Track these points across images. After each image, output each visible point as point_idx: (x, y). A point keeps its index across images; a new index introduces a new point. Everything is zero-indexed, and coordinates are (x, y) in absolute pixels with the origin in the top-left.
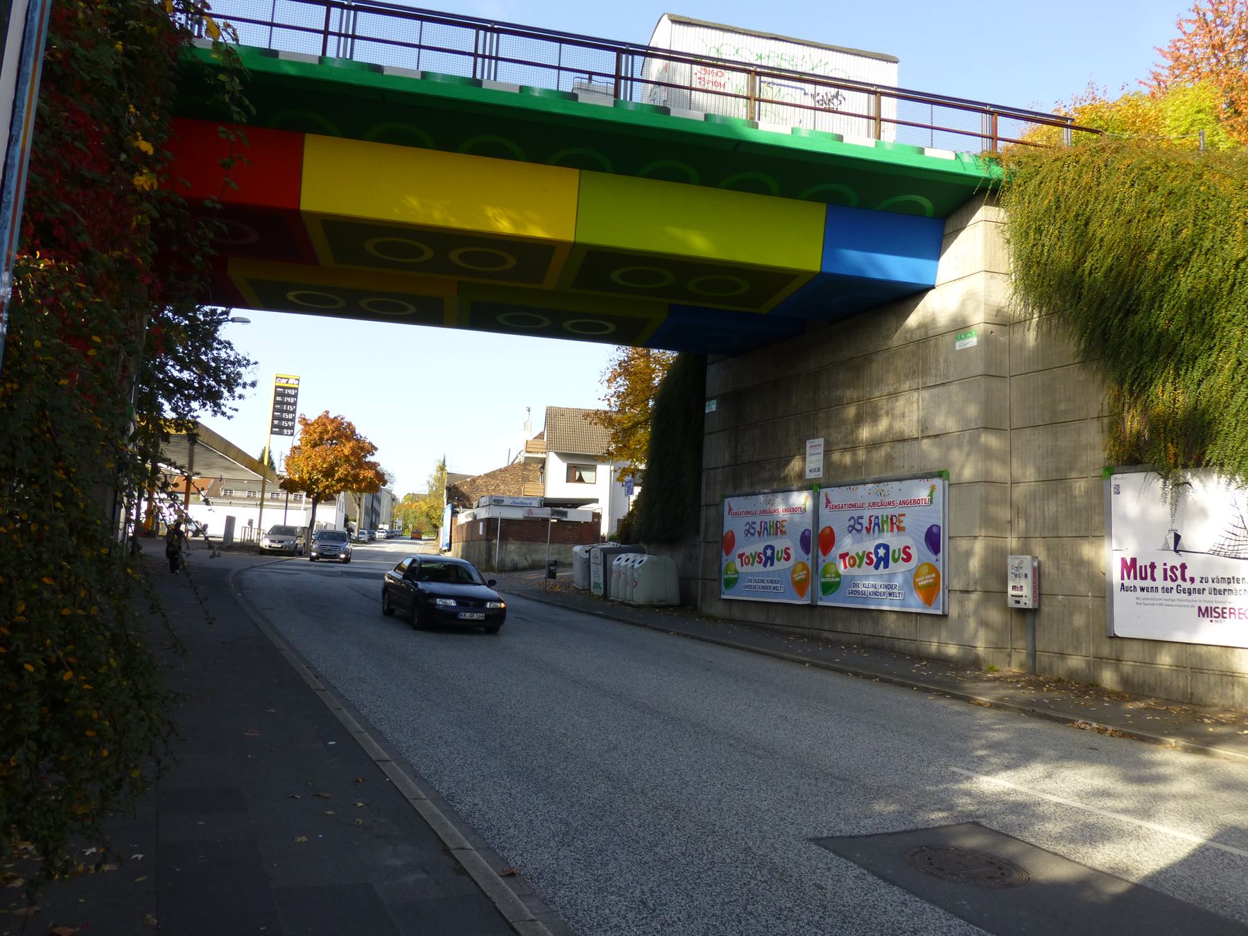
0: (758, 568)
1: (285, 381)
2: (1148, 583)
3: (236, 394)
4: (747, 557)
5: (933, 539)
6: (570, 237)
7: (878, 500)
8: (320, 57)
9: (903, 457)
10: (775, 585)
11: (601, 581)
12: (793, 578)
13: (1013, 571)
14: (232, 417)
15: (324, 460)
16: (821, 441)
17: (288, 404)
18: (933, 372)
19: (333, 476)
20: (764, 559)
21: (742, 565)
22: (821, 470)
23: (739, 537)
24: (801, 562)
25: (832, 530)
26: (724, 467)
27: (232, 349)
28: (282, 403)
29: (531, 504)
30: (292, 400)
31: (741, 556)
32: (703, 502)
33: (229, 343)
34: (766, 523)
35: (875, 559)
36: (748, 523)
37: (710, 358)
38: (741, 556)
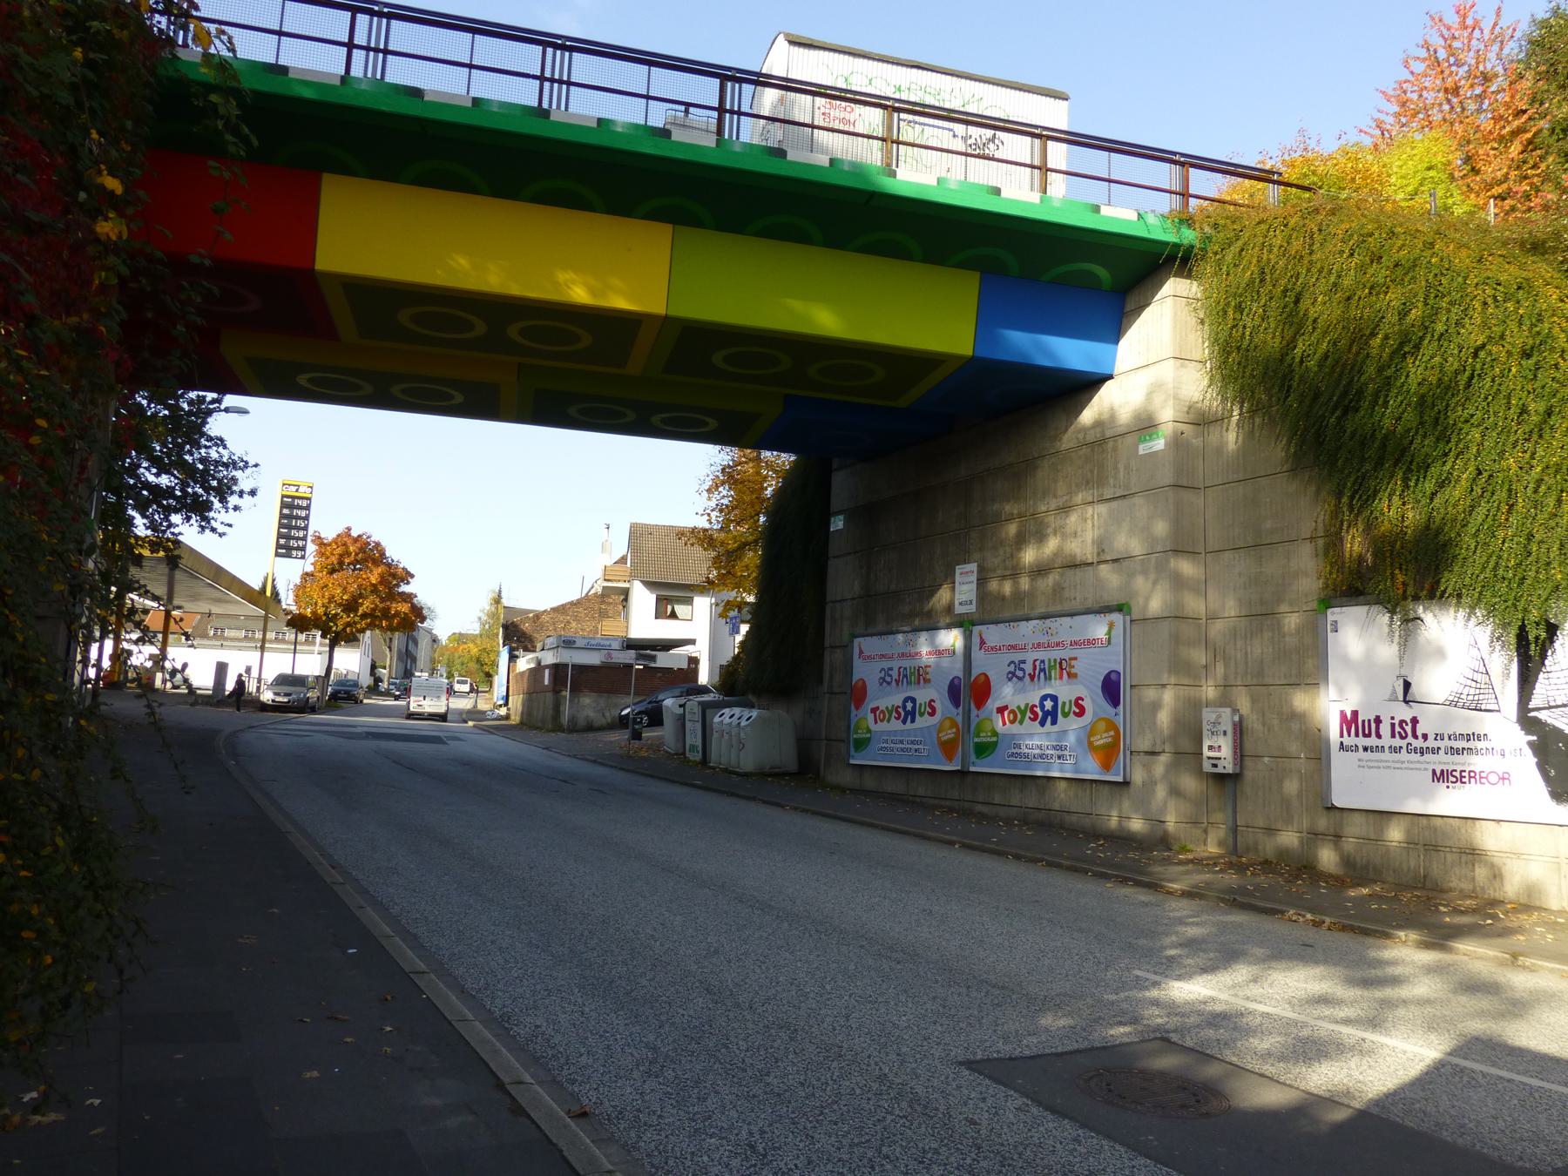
0: (896, 725)
1: (294, 488)
2: (1372, 741)
3: (230, 505)
4: (882, 712)
5: (1111, 689)
7: (1044, 640)
8: (342, 77)
9: (1075, 586)
10: (917, 747)
11: (699, 743)
12: (939, 738)
13: (1208, 727)
14: (224, 534)
15: (345, 590)
16: (973, 567)
17: (298, 518)
18: (1111, 481)
19: (356, 611)
20: (903, 714)
21: (876, 722)
22: (974, 602)
23: (873, 686)
24: (949, 718)
25: (864, 682)
26: (853, 599)
27: (225, 447)
28: (290, 517)
29: (610, 646)
30: (303, 513)
31: (874, 710)
32: (827, 644)
33: (221, 440)
34: (905, 669)
35: (1040, 714)
36: (883, 669)
37: (835, 463)
38: (874, 710)
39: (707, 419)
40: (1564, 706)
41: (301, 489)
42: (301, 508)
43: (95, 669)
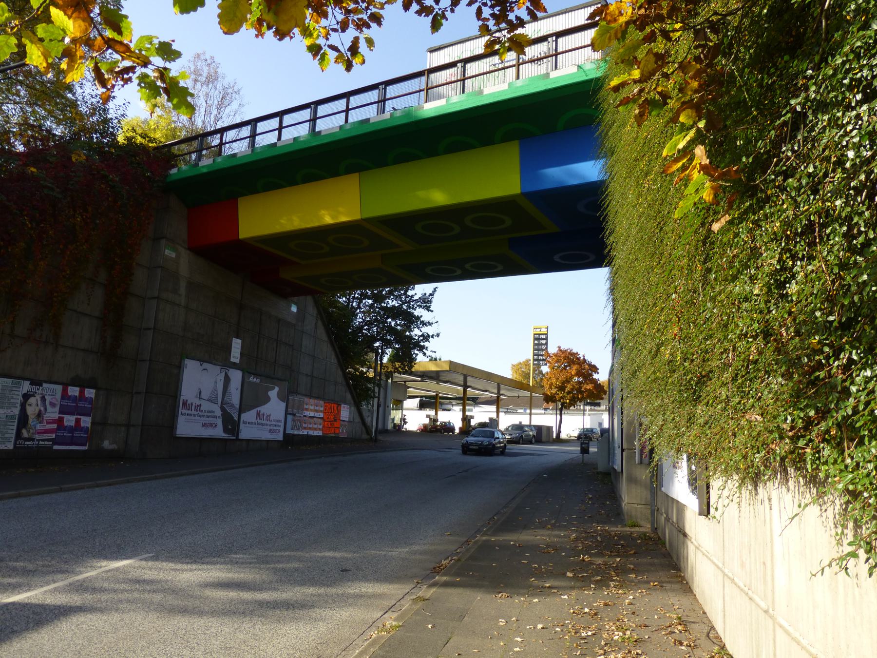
1: (539, 330)
2: (189, 412)
6: (357, 217)
15: (557, 379)
17: (542, 344)
19: (564, 390)
28: (538, 345)
30: (544, 342)
39: (431, 273)
40: (775, 655)
42: (543, 339)
43: (73, 424)
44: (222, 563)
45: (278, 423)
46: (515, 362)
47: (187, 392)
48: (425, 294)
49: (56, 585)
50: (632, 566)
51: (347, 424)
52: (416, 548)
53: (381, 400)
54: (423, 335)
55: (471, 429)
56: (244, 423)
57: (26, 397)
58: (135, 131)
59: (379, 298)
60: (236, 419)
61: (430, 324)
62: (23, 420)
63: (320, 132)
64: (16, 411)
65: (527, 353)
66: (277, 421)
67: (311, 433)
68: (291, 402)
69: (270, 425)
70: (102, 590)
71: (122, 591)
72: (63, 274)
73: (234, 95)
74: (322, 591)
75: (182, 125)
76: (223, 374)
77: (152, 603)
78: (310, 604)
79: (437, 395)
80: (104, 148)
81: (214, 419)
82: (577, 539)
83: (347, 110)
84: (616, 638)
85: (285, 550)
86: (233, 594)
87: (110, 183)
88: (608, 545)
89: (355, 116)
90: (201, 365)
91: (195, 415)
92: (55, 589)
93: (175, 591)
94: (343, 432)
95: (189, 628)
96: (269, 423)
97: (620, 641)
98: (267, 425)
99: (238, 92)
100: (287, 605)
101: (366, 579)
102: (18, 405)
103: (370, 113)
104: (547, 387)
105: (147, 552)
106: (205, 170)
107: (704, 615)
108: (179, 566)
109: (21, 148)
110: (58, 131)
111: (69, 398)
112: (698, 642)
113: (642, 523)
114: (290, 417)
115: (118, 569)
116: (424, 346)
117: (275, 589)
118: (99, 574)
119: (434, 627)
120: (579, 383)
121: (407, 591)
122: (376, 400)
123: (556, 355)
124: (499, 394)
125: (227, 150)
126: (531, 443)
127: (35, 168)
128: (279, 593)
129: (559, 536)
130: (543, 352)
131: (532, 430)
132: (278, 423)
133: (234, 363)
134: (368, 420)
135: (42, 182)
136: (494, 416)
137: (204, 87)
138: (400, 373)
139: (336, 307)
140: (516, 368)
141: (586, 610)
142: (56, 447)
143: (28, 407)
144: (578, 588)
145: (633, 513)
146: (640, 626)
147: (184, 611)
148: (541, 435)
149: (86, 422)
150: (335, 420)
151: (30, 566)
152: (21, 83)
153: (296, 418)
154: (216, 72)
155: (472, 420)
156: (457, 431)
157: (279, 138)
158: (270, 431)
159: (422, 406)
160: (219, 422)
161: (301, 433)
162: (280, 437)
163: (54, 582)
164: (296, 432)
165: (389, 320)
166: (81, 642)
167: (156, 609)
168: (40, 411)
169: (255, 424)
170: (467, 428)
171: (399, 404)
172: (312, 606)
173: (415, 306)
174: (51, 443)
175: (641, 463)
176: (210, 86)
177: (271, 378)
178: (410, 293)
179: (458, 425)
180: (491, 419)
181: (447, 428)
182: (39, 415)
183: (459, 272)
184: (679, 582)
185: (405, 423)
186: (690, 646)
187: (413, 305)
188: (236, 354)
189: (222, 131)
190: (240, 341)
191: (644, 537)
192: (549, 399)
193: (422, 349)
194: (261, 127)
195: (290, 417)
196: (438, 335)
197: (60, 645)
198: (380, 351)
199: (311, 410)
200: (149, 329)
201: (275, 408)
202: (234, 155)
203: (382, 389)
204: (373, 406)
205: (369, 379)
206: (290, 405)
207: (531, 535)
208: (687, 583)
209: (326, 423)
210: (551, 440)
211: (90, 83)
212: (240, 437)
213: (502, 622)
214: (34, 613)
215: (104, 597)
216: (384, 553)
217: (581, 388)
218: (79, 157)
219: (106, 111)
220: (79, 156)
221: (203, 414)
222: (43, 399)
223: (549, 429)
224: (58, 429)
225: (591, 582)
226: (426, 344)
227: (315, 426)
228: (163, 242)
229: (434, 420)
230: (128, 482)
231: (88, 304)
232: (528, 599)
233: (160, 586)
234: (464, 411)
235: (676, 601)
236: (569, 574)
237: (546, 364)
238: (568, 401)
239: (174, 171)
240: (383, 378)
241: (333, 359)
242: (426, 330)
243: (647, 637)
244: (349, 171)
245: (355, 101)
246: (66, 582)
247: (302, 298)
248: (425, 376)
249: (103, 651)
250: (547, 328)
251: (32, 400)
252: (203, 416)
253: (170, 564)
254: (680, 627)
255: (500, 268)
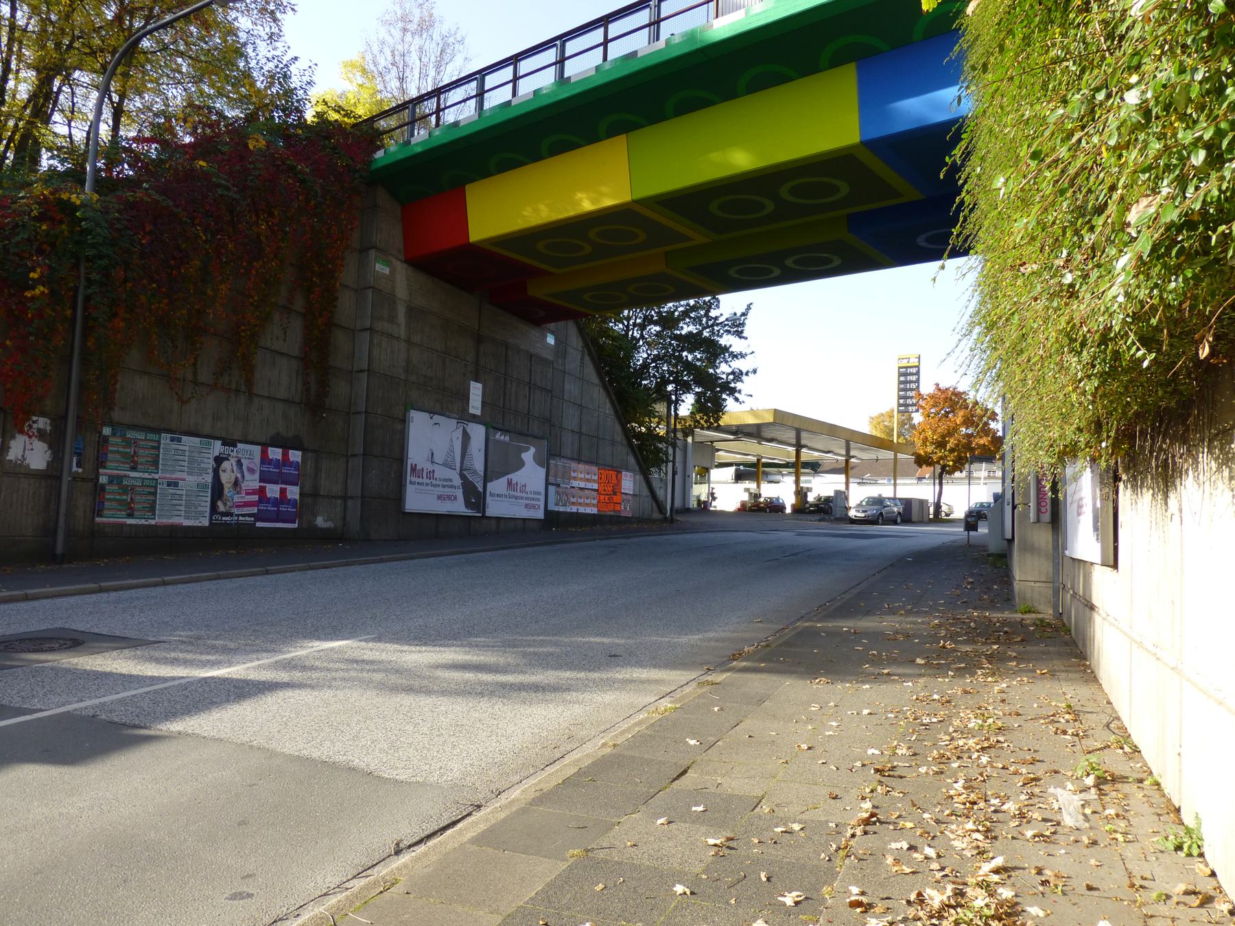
1: (906, 361)
2: (420, 480)
15: (934, 432)
17: (911, 382)
28: (905, 382)
30: (914, 378)
39: (736, 276)
41: (911, 361)
43: (278, 496)
44: (458, 646)
45: (536, 496)
46: (875, 414)
47: (416, 454)
48: (735, 314)
49: (261, 662)
50: (1014, 654)
51: (630, 497)
52: (711, 635)
53: (679, 466)
54: (733, 373)
55: (807, 505)
56: (491, 495)
57: (219, 460)
58: (326, 104)
59: (668, 322)
60: (481, 489)
61: (743, 356)
62: (217, 490)
63: (569, 78)
64: (209, 478)
65: (888, 400)
66: (535, 493)
67: (582, 510)
68: (552, 466)
69: (527, 498)
70: (313, 668)
71: (337, 670)
72: (251, 300)
73: (457, 46)
74: (582, 675)
75: (390, 96)
76: (459, 433)
77: (371, 681)
78: (564, 687)
79: (758, 460)
80: (287, 129)
81: (453, 490)
82: (940, 626)
83: (606, 43)
84: (970, 726)
85: (538, 635)
86: (469, 676)
87: (299, 176)
88: (986, 632)
89: (617, 50)
90: (431, 418)
91: (427, 485)
92: (259, 666)
93: (399, 671)
94: (626, 510)
95: (414, 705)
96: (524, 495)
97: (977, 728)
98: (522, 498)
99: (461, 42)
100: (536, 688)
101: (640, 664)
102: (210, 471)
103: (639, 43)
104: (919, 443)
105: (368, 633)
106: (419, 149)
107: (1108, 706)
108: (406, 648)
109: (188, 139)
110: (230, 114)
111: (270, 462)
112: (1089, 733)
113: (1041, 608)
114: (552, 489)
115: (332, 649)
116: (735, 388)
117: (522, 672)
118: (311, 653)
119: (721, 709)
120: (969, 436)
121: (693, 678)
122: (670, 465)
123: (932, 396)
124: (848, 456)
125: (449, 117)
126: (895, 523)
127: (203, 160)
128: (527, 676)
129: (915, 623)
130: (913, 394)
131: (896, 505)
132: (536, 496)
133: (474, 415)
134: (660, 493)
135: (214, 180)
136: (842, 488)
137: (417, 37)
138: (702, 428)
139: (608, 337)
140: (877, 420)
141: (936, 697)
142: (259, 524)
143: (221, 473)
144: (929, 675)
145: (1028, 595)
146: (1010, 715)
147: (409, 690)
148: (909, 512)
149: (293, 492)
150: (615, 493)
151: (232, 645)
152: (182, 54)
153: (560, 490)
154: (431, 15)
155: (809, 494)
156: (788, 510)
157: (514, 94)
158: (527, 506)
159: (739, 477)
160: (459, 493)
161: (568, 510)
162: (540, 515)
163: (258, 659)
164: (562, 509)
165: (685, 354)
166: (287, 714)
167: (375, 687)
168: (237, 478)
169: (506, 496)
170: (802, 508)
171: (704, 473)
172: (568, 689)
173: (722, 331)
174: (253, 519)
175: (1038, 521)
176: (424, 36)
177: (524, 436)
178: (713, 313)
179: (789, 500)
180: (837, 492)
181: (775, 507)
182: (236, 484)
183: (777, 272)
184: (1080, 671)
185: (714, 499)
186: (1077, 735)
187: (718, 331)
188: (475, 404)
189: (438, 92)
190: (480, 386)
191: (1042, 624)
192: (921, 461)
193: (732, 391)
194: (490, 81)
195: (552, 489)
196: (755, 371)
197: (264, 717)
198: (673, 397)
199: (581, 479)
200: (362, 371)
201: (531, 475)
202: (456, 124)
203: (677, 449)
204: (666, 474)
205: (661, 439)
206: (552, 473)
207: (874, 622)
208: (1092, 672)
209: (602, 497)
210: (926, 519)
211: (265, 43)
212: (487, 514)
213: (814, 708)
214: (235, 686)
215: (315, 675)
216: (667, 639)
217: (970, 442)
218: (257, 143)
219: (286, 76)
220: (257, 141)
221: (438, 483)
222: (239, 463)
223: (923, 503)
224: (260, 501)
225: (949, 669)
226: (739, 385)
227: (588, 501)
228: (373, 253)
229: (756, 495)
230: (347, 564)
231: (285, 340)
232: (857, 685)
233: (381, 666)
234: (797, 482)
235: (1070, 691)
236: (919, 661)
237: (917, 411)
238: (951, 463)
239: (380, 154)
240: (680, 435)
241: (608, 409)
242: (737, 364)
243: (1016, 725)
244: (613, 132)
245: (615, 28)
246: (272, 660)
247: (561, 324)
248: (740, 432)
249: (312, 723)
250: (919, 358)
251: (226, 465)
252: (438, 486)
253: (395, 646)
254: (1067, 716)
255: (837, 262)
